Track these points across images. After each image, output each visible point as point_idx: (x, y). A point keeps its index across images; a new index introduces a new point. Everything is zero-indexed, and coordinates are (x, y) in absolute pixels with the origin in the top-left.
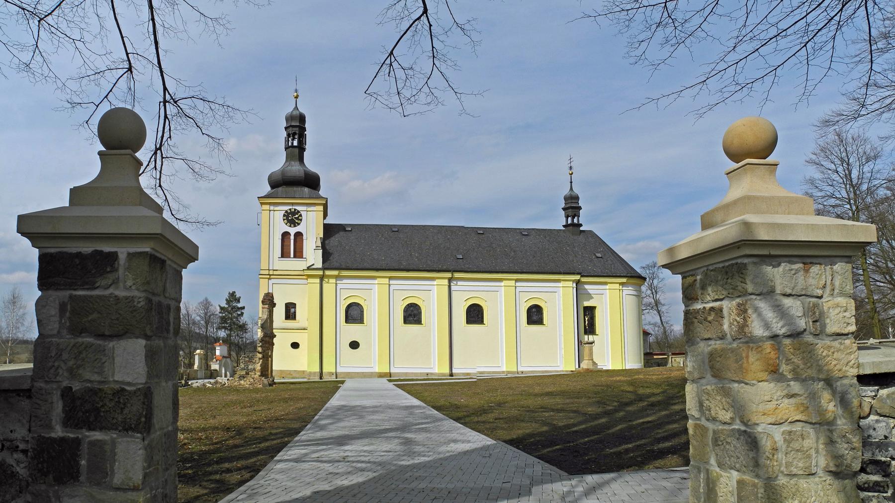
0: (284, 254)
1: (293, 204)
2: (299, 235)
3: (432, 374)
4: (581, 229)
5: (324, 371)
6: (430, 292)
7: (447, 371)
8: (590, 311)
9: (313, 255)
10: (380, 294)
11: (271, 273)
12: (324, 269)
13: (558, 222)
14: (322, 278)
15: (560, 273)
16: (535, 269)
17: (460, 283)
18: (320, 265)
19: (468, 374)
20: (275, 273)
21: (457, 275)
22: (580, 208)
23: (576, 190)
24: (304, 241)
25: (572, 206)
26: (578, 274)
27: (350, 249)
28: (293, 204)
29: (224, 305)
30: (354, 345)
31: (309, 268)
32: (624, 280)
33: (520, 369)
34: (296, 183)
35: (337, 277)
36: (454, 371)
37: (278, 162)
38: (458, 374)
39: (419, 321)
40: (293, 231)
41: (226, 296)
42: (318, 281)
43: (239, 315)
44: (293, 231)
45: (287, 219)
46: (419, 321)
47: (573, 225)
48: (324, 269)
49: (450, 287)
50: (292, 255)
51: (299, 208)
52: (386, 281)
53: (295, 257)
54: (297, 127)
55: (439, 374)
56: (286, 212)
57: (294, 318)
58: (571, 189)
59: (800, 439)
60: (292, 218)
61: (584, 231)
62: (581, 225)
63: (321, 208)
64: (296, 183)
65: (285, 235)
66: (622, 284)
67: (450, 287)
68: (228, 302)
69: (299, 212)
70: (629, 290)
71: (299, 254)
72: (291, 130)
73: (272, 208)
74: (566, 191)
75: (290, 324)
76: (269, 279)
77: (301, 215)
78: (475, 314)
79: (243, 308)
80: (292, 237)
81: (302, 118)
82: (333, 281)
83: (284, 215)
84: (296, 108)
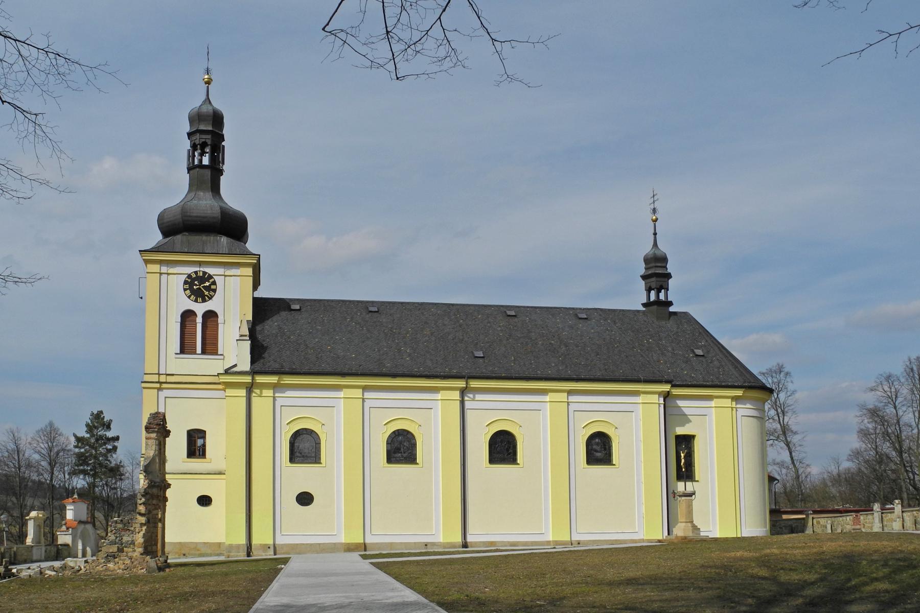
0: (185, 347)
1: (200, 264)
2: (210, 316)
3: (433, 544)
4: (672, 309)
6: (432, 411)
7: (458, 539)
8: (685, 442)
9: (234, 349)
10: (350, 414)
11: (163, 378)
12: (254, 372)
13: (634, 298)
14: (250, 388)
15: (638, 381)
17: (479, 397)
18: (246, 365)
19: (492, 543)
20: (170, 379)
21: (474, 384)
23: (663, 247)
25: (657, 272)
27: (294, 340)
28: (200, 264)
29: (83, 433)
30: (305, 499)
31: (227, 372)
32: (739, 393)
33: (576, 538)
34: (205, 228)
35: (275, 387)
36: (470, 539)
40: (200, 309)
41: (87, 419)
42: (243, 392)
43: (109, 451)
44: (200, 309)
45: (191, 289)
47: (658, 302)
48: (254, 372)
49: (462, 403)
50: (199, 350)
51: (211, 271)
53: (204, 352)
56: (189, 276)
57: (203, 454)
58: (655, 244)
60: (199, 287)
61: (675, 313)
62: (670, 304)
63: (249, 271)
64: (205, 228)
65: (187, 316)
66: (736, 399)
67: (462, 403)
68: (90, 428)
69: (210, 277)
71: (210, 347)
72: (198, 138)
73: (164, 269)
75: (196, 464)
76: (159, 389)
77: (214, 283)
78: (503, 448)
79: (117, 439)
80: (199, 320)
82: (268, 393)
83: (186, 283)
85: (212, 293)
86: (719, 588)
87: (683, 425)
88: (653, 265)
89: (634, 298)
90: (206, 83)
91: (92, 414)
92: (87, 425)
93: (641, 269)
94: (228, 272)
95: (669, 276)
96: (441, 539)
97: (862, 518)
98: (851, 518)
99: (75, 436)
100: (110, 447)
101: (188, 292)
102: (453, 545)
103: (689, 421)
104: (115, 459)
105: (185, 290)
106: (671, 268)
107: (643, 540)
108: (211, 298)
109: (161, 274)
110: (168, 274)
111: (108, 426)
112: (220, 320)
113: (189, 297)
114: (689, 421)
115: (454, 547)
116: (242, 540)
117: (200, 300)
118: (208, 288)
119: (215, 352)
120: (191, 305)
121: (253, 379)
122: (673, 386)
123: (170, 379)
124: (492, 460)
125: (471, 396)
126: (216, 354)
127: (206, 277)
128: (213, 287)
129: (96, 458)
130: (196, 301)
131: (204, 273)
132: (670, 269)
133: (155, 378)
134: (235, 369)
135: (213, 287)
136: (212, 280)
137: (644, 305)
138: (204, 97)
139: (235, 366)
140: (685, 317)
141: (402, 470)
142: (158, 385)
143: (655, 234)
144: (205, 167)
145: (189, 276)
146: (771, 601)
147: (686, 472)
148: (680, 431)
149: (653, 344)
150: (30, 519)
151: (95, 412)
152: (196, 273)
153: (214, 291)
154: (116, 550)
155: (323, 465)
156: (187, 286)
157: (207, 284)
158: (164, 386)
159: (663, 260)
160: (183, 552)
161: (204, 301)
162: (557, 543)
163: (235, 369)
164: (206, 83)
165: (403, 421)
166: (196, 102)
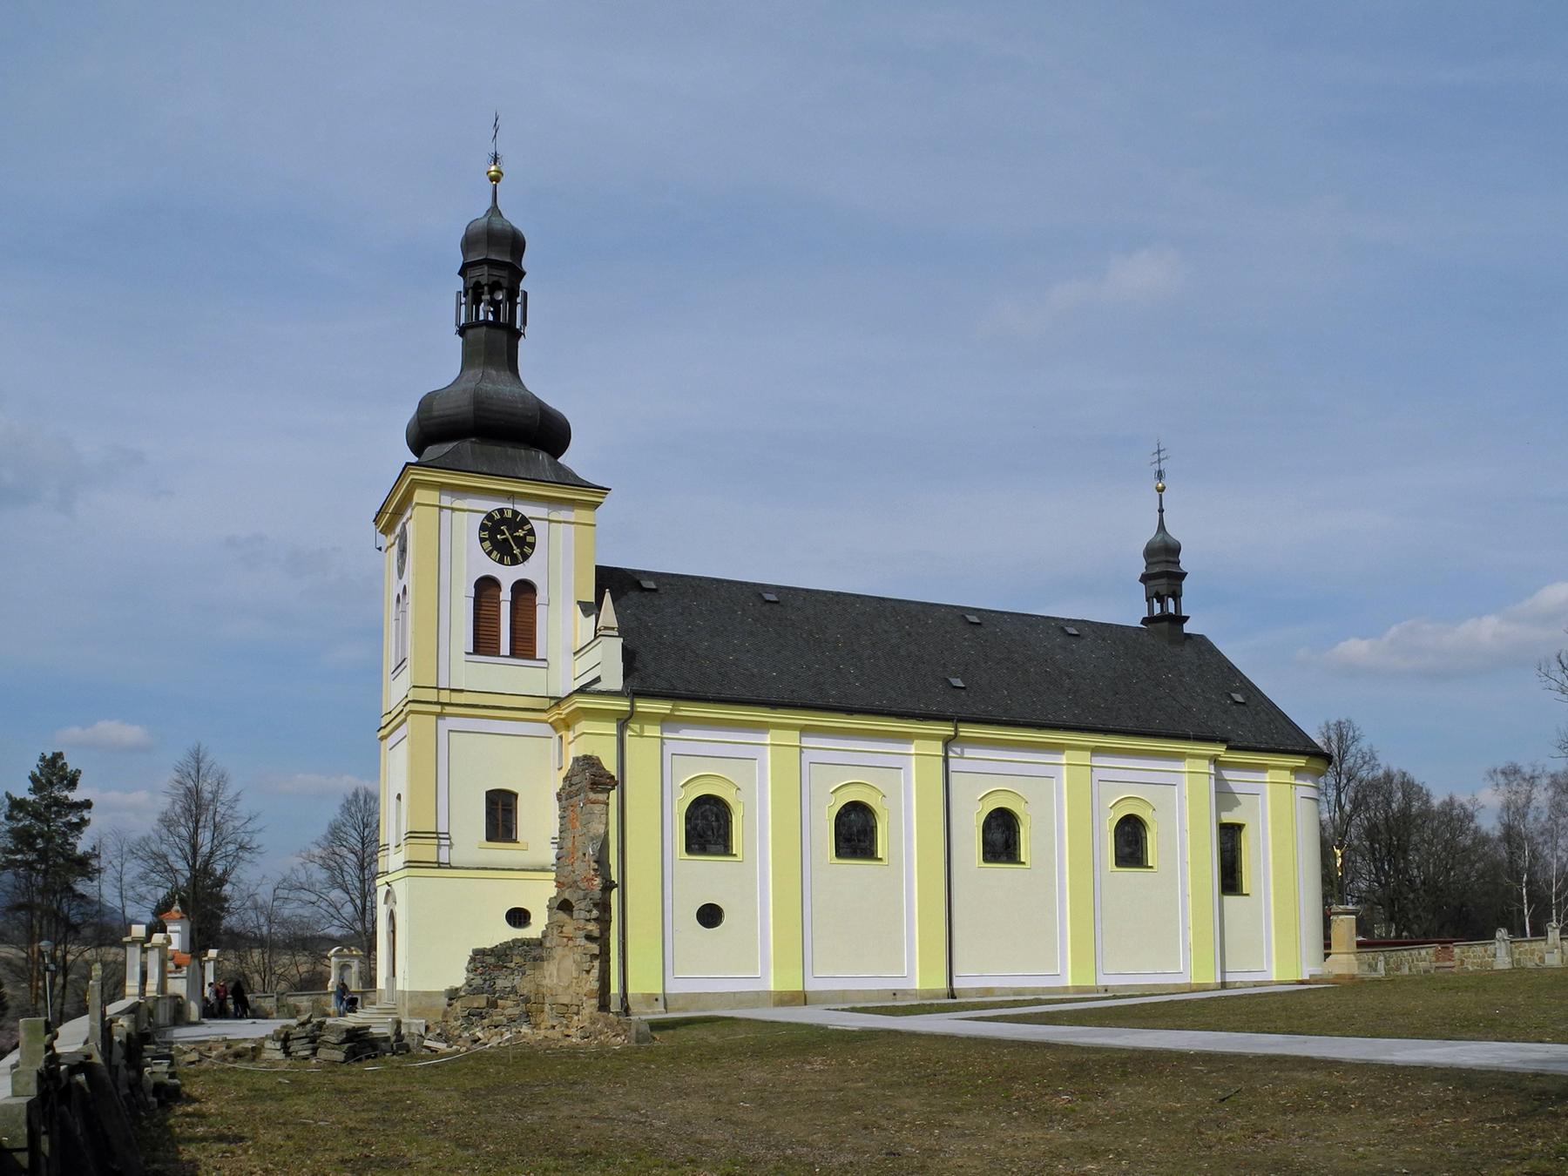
0: (484, 643)
1: (511, 496)
2: (524, 590)
3: (905, 992)
5: (630, 991)
6: (903, 773)
7: (942, 984)
8: (1230, 835)
10: (777, 771)
11: (445, 697)
13: (1130, 609)
14: (624, 721)
15: (1185, 737)
16: (1131, 725)
17: (969, 752)
18: (614, 679)
19: (988, 991)
20: (457, 698)
21: (966, 731)
22: (1183, 575)
23: (1175, 532)
24: (541, 612)
25: (1163, 569)
26: (1223, 741)
27: (700, 643)
28: (511, 496)
29: (23, 791)
30: (710, 916)
31: (582, 691)
32: (1300, 762)
33: (674, 988)
34: (492, 434)
35: (665, 721)
36: (955, 986)
38: (966, 992)
39: (725, 848)
40: (507, 576)
41: (33, 765)
42: (612, 728)
43: (69, 825)
44: (507, 576)
45: (492, 539)
46: (725, 848)
47: (1165, 617)
49: (946, 760)
50: (505, 647)
51: (526, 510)
52: (793, 737)
53: (513, 654)
54: (494, 270)
55: (1078, 989)
56: (489, 516)
58: (1161, 526)
60: (506, 537)
61: (1189, 636)
64: (492, 434)
65: (486, 587)
66: (1296, 771)
67: (946, 760)
68: (37, 784)
69: (525, 521)
70: (1305, 787)
71: (524, 646)
72: (483, 275)
73: (446, 500)
74: (1149, 533)
75: (501, 853)
76: (440, 715)
77: (531, 532)
78: (1002, 837)
79: (87, 805)
80: (506, 595)
81: (516, 244)
82: (653, 730)
83: (483, 527)
84: (494, 209)
85: (527, 550)
87: (1230, 810)
88: (1163, 558)
89: (1130, 609)
90: (492, 179)
91: (43, 758)
92: (34, 779)
93: (1141, 566)
94: (554, 516)
95: (1183, 575)
96: (1194, 979)
97: (1456, 950)
98: (1431, 951)
99: (8, 796)
100: (75, 820)
101: (487, 544)
102: (934, 994)
103: (1238, 803)
104: (83, 845)
105: (482, 540)
107: (1270, 983)
108: (526, 557)
109: (441, 508)
110: (453, 509)
111: (72, 782)
112: (540, 597)
113: (489, 554)
114: (1238, 803)
117: (507, 559)
118: (521, 542)
119: (531, 655)
121: (632, 706)
122: (1229, 748)
124: (839, 854)
125: (958, 750)
126: (532, 657)
127: (518, 522)
128: (529, 539)
129: (49, 839)
130: (501, 561)
131: (516, 513)
132: (1184, 566)
133: (431, 695)
134: (598, 687)
135: (529, 539)
137: (1144, 621)
138: (488, 204)
139: (598, 680)
140: (1200, 642)
141: (856, 868)
142: (438, 709)
143: (1161, 511)
144: (486, 323)
145: (489, 516)
147: (1230, 880)
148: (1228, 818)
149: (1147, 677)
150: (152, 948)
151: (49, 756)
152: (501, 511)
153: (532, 546)
154: (484, 1003)
155: (739, 858)
156: (485, 534)
157: (521, 533)
158: (448, 710)
161: (515, 562)
163: (598, 687)
164: (492, 179)
165: (859, 788)
166: (478, 210)
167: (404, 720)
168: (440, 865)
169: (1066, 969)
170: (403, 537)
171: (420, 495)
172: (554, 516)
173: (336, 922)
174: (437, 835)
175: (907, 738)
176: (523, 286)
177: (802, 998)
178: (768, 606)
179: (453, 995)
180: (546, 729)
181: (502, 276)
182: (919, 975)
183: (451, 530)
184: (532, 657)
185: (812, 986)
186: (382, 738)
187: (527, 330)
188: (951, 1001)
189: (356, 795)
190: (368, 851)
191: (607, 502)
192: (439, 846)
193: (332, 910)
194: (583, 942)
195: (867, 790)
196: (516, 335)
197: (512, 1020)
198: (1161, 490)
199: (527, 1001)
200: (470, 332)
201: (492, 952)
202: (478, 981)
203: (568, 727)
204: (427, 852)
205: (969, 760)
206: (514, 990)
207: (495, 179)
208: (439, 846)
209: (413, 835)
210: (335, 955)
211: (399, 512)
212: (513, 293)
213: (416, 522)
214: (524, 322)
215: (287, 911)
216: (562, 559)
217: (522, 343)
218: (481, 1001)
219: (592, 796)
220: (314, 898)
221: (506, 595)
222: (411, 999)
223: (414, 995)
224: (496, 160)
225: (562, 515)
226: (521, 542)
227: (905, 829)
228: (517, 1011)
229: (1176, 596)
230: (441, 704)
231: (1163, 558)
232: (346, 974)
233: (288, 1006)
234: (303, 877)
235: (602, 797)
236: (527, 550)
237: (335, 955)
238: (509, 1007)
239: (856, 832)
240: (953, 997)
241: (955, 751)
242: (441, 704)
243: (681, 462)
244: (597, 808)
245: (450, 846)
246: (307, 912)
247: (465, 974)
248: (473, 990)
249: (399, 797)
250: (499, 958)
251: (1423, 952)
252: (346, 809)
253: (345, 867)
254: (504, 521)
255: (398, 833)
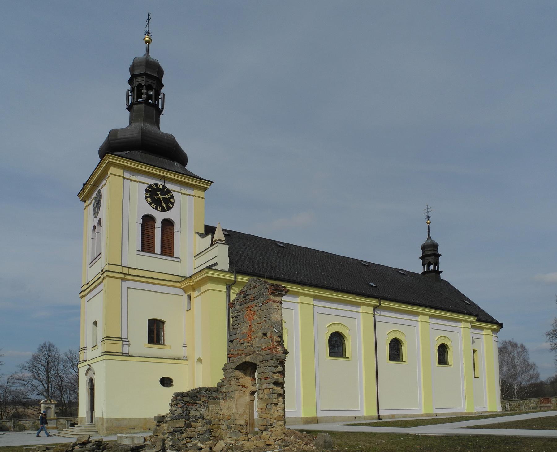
0: (147, 246)
2: (168, 224)
3: (360, 417)
6: (358, 319)
11: (126, 271)
17: (383, 313)
18: (224, 263)
19: (393, 416)
20: (132, 272)
21: (384, 304)
23: (435, 239)
24: (175, 235)
25: (430, 254)
26: (476, 316)
31: (209, 268)
36: (380, 414)
37: (121, 120)
40: (159, 216)
45: (152, 197)
47: (429, 272)
51: (169, 186)
52: (310, 300)
53: (162, 253)
54: (146, 83)
56: (150, 186)
58: (429, 237)
59: (304, 443)
60: (159, 197)
65: (148, 220)
69: (169, 191)
71: (168, 249)
73: (127, 175)
74: (423, 240)
75: (155, 350)
76: (123, 280)
77: (172, 197)
78: (395, 349)
80: (158, 225)
83: (147, 191)
85: (170, 205)
86: (420, 445)
88: (432, 249)
89: (417, 267)
90: (146, 42)
94: (183, 191)
98: (537, 400)
101: (149, 199)
102: (372, 418)
105: (146, 197)
106: (440, 251)
108: (169, 209)
109: (124, 178)
110: (131, 180)
113: (150, 204)
115: (373, 419)
116: (376, 414)
117: (160, 208)
120: (151, 211)
121: (236, 278)
123: (132, 272)
125: (379, 312)
126: (172, 256)
128: (171, 200)
130: (156, 209)
131: (164, 187)
132: (440, 252)
133: (119, 269)
134: (216, 267)
135: (171, 200)
136: (170, 194)
138: (144, 52)
139: (216, 264)
142: (122, 276)
143: (429, 231)
146: (222, 450)
152: (156, 185)
153: (173, 204)
154: (182, 424)
156: (148, 195)
157: (167, 197)
158: (128, 277)
159: (435, 246)
160: (148, 427)
161: (163, 210)
162: (428, 415)
167: (102, 282)
168: (123, 354)
169: (423, 408)
170: (99, 195)
171: (112, 170)
172: (183, 191)
173: (35, 392)
174: (121, 339)
175: (358, 305)
176: (162, 91)
177: (315, 420)
178: (281, 249)
179: (160, 420)
180: (180, 291)
181: (154, 83)
182: (366, 410)
183: (127, 192)
184: (172, 256)
185: (320, 415)
186: (81, 297)
187: (164, 111)
188: (379, 421)
189: (45, 344)
190: (50, 366)
191: (211, 187)
192: (123, 345)
193: (33, 387)
194: (272, 386)
195: (341, 327)
196: (160, 112)
197: (200, 434)
198: (429, 223)
199: (210, 423)
200: (135, 107)
201: (188, 394)
202: (179, 411)
203: (194, 290)
204: (116, 347)
205: (384, 316)
206: (201, 417)
207: (148, 42)
208: (123, 345)
209: (108, 339)
210: (43, 403)
211: (96, 184)
212: (158, 93)
213: (109, 189)
214: (163, 107)
215: (13, 388)
216: (187, 211)
217: (161, 116)
218: (181, 423)
219: (272, 297)
220: (26, 383)
221: (158, 225)
222: (107, 422)
223: (109, 420)
224: (148, 33)
225: (188, 191)
226: (167, 201)
227: (357, 344)
228: (203, 429)
229: (437, 263)
230: (124, 275)
231: (432, 249)
232: (49, 411)
233: (18, 425)
234: (20, 375)
235: (278, 299)
236: (170, 205)
237: (43, 403)
238: (199, 427)
239: (337, 344)
240: (380, 419)
241: (378, 312)
242: (124, 275)
243: (253, 172)
244: (275, 305)
245: (129, 345)
246: (22, 388)
247: (169, 407)
248: (175, 417)
249: (95, 323)
250: (192, 398)
251: (532, 401)
252: (41, 349)
253: (39, 372)
254: (157, 189)
255: (95, 339)
